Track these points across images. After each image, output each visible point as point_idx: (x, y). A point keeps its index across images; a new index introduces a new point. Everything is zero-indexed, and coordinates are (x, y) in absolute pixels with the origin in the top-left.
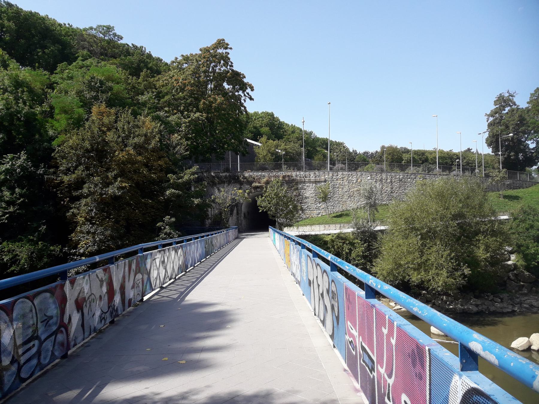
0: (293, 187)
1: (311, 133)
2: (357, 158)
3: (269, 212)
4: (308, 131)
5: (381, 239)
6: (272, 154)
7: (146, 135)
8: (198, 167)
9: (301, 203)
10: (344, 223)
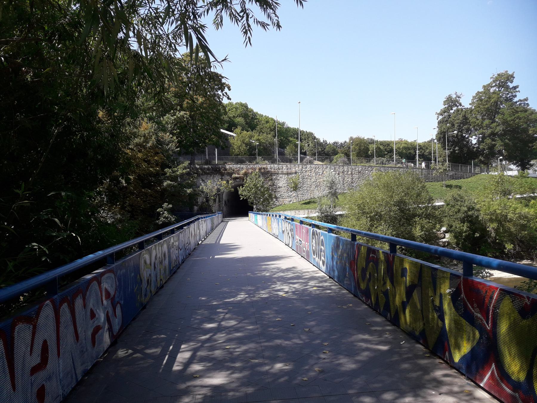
0: (269, 178)
1: (283, 124)
2: (327, 149)
3: (249, 200)
4: (281, 122)
5: (340, 221)
6: (247, 145)
7: (144, 136)
8: (189, 162)
9: (275, 192)
10: (311, 209)
